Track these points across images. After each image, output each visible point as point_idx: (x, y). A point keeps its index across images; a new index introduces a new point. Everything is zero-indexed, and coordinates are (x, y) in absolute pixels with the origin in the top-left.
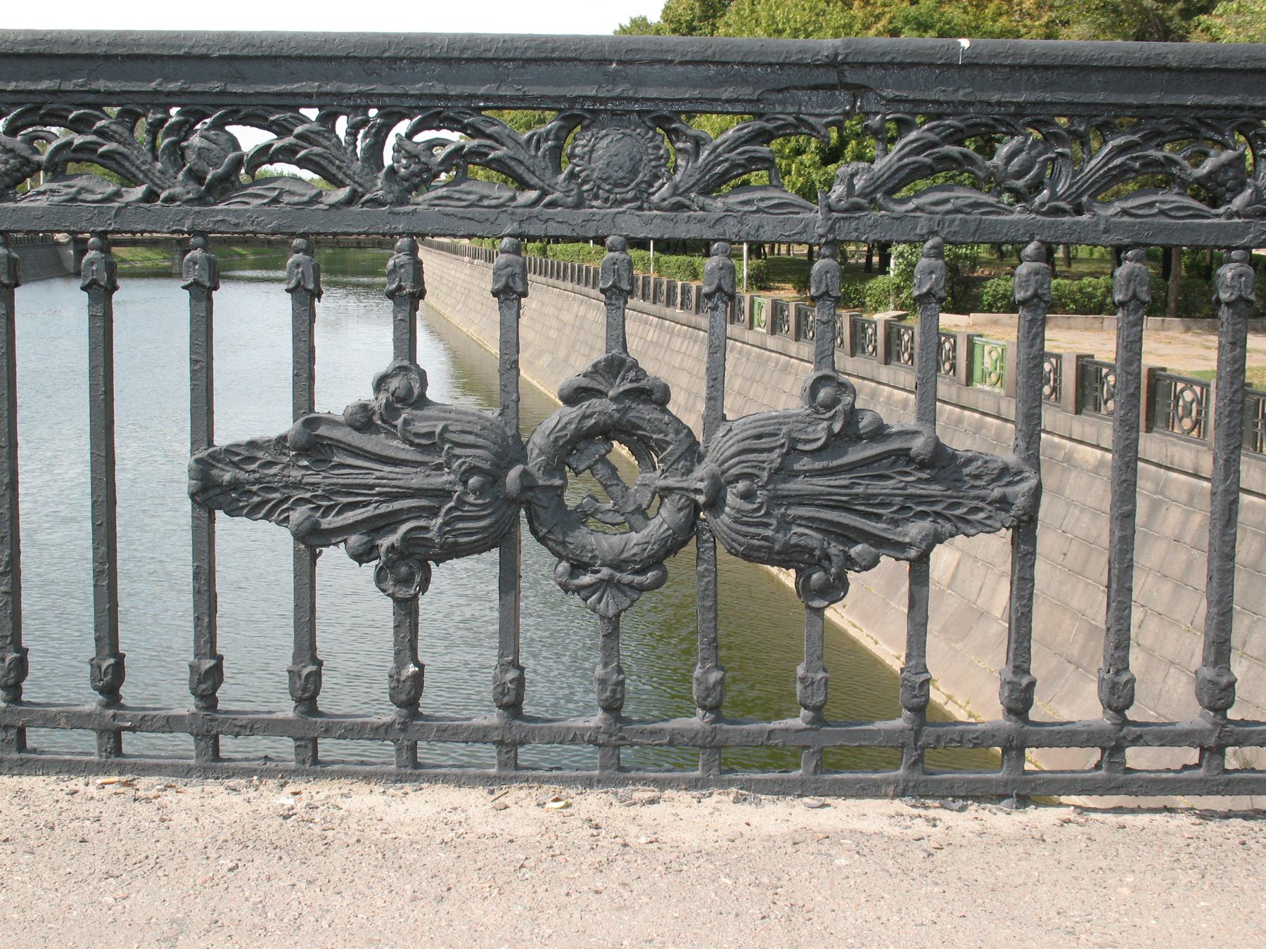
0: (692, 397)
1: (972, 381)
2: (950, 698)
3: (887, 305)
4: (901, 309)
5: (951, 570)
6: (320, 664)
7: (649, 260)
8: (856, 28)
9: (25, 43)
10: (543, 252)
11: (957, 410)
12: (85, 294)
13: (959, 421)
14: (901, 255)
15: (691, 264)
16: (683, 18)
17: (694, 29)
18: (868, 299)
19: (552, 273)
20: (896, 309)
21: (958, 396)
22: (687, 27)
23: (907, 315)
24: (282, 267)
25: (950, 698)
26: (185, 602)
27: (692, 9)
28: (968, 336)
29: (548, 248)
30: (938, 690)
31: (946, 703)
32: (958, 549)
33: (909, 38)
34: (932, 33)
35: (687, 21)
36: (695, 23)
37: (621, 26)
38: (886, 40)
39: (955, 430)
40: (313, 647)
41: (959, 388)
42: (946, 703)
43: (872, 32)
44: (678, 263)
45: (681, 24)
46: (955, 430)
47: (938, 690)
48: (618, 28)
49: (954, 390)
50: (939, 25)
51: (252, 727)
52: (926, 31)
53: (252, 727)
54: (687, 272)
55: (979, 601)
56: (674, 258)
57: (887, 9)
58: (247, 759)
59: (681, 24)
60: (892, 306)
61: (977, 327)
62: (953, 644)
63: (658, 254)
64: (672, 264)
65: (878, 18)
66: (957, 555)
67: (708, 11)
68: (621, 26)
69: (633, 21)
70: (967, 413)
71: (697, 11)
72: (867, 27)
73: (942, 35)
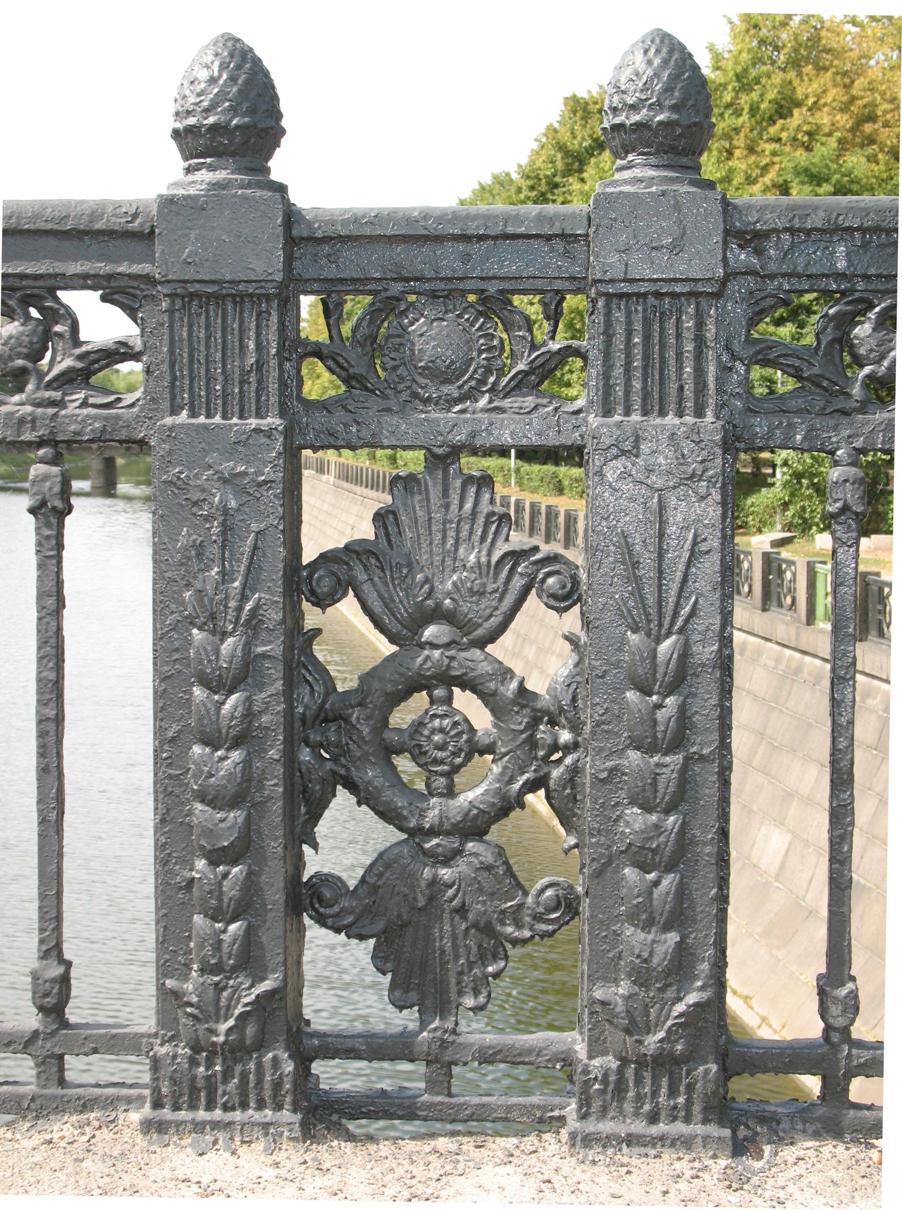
0: (520, 640)
1: (815, 619)
2: (764, 1019)
3: (772, 525)
4: (789, 530)
5: (780, 857)
6: (69, 964)
7: (509, 470)
8: (735, 182)
9: (345, 223)
10: (393, 460)
11: (798, 655)
12: (31, 518)
13: (799, 670)
14: (785, 463)
15: (555, 475)
16: (542, 173)
17: (556, 186)
18: (751, 517)
19: (384, 487)
20: (783, 530)
21: (797, 639)
22: (548, 184)
23: (794, 537)
24: (25, 479)
25: (764, 1019)
26: (31, 887)
27: (552, 162)
28: (808, 563)
29: (398, 456)
30: (752, 1009)
31: (759, 1027)
32: (789, 831)
33: (800, 193)
34: (827, 187)
35: (546, 177)
36: (557, 179)
37: (480, 184)
38: (772, 198)
39: (794, 681)
40: (58, 947)
41: (798, 628)
42: (759, 1027)
43: (757, 188)
44: (541, 474)
45: (540, 180)
46: (794, 681)
47: (752, 1009)
48: (477, 187)
49: (792, 630)
50: (837, 176)
51: (540, 1052)
52: (819, 185)
53: (540, 1052)
54: (551, 486)
55: (808, 897)
56: (536, 468)
57: (776, 159)
58: (98, 1086)
59: (540, 180)
60: (779, 527)
61: (879, 553)
62: (774, 952)
63: (519, 462)
64: (534, 476)
65: (765, 169)
66: (788, 838)
67: (572, 164)
68: (480, 184)
69: (495, 177)
70: (807, 659)
71: (560, 165)
72: (751, 181)
73: (840, 190)
